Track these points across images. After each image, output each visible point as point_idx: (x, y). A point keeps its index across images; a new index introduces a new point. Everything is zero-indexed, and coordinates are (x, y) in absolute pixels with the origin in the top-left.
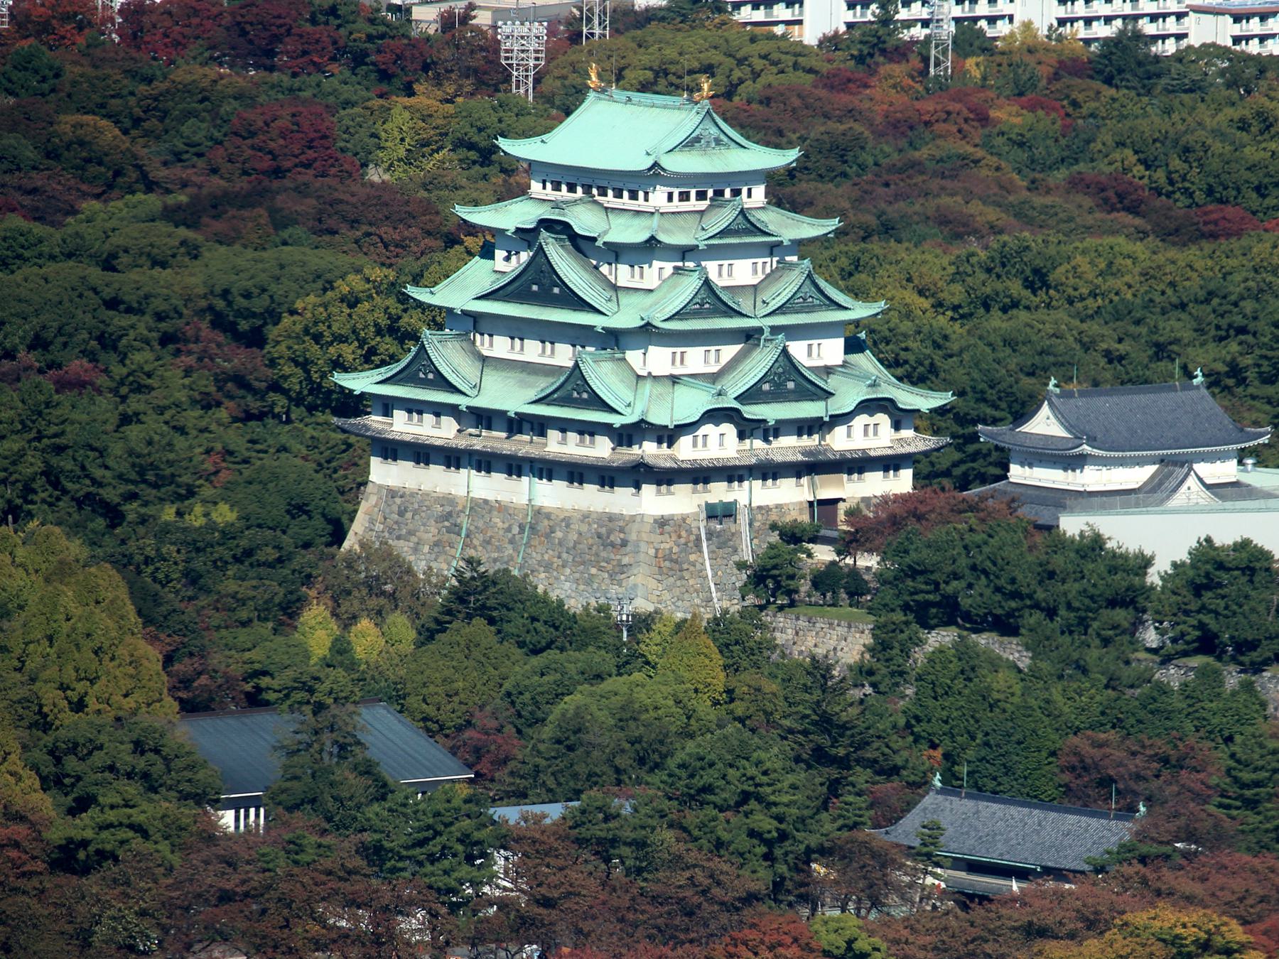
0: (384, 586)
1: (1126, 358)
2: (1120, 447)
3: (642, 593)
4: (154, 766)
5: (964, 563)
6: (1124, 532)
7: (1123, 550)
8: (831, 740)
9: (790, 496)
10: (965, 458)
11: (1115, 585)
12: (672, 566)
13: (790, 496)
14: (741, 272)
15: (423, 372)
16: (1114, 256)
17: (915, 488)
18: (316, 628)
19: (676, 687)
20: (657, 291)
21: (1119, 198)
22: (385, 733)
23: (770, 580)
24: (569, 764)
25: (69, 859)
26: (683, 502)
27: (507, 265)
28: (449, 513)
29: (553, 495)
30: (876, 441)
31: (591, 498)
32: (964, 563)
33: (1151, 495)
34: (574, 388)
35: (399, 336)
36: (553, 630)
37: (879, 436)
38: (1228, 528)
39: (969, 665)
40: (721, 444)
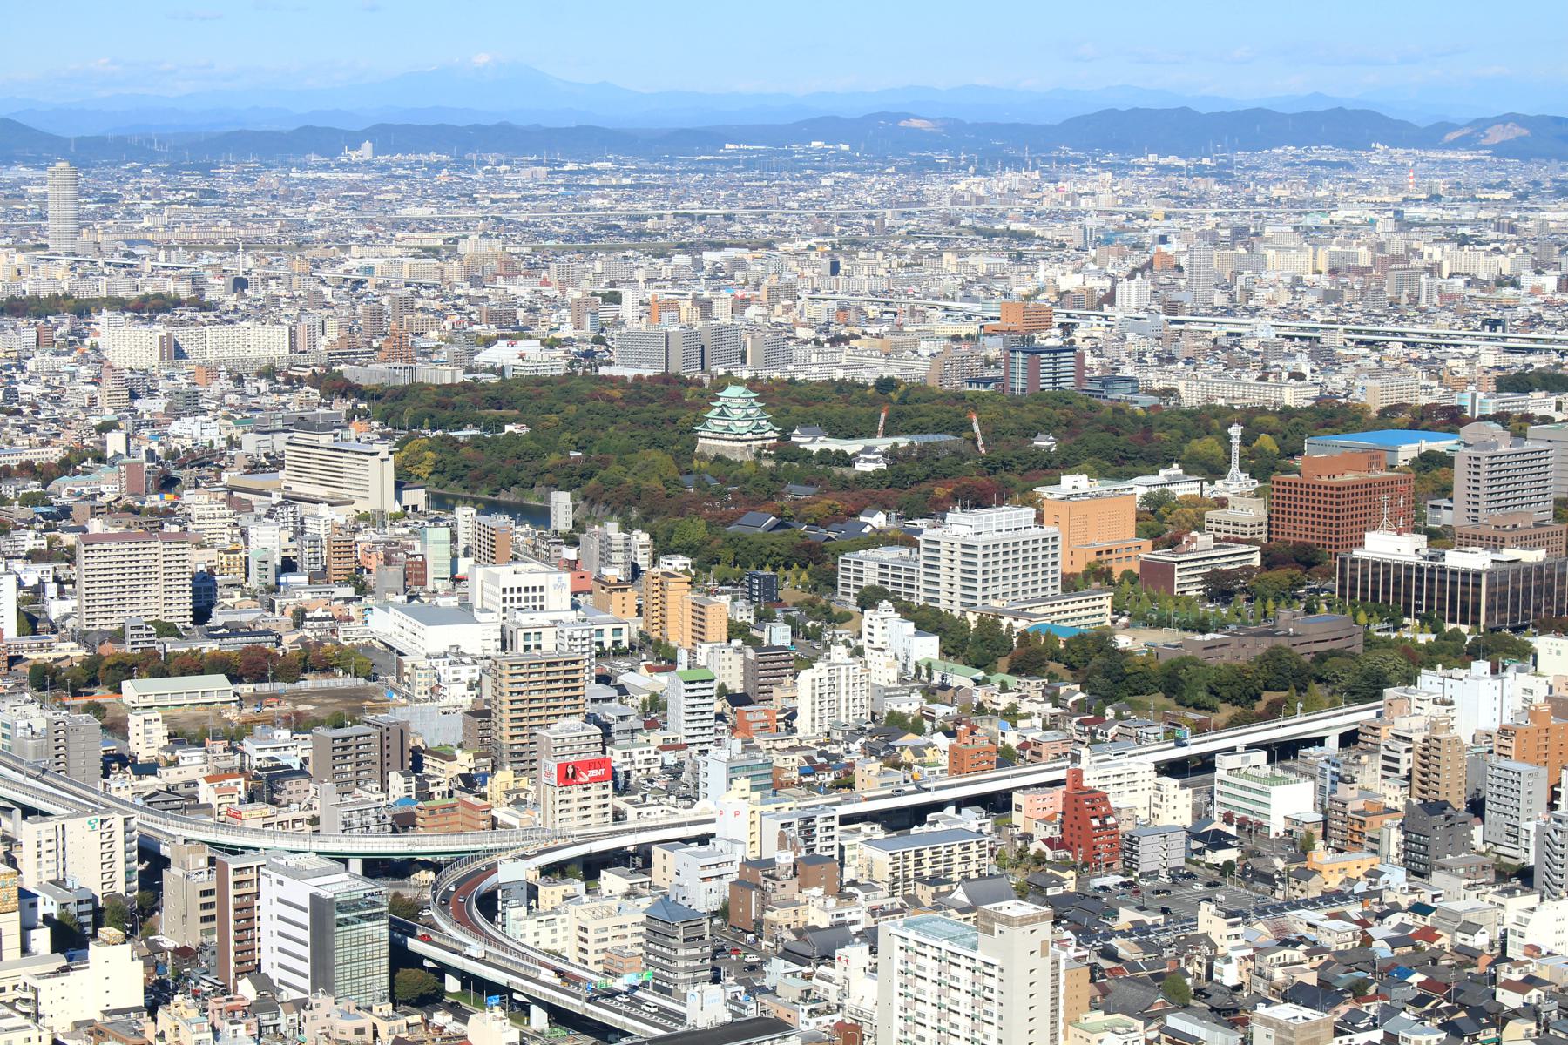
0: (703, 457)
1: (805, 423)
2: (806, 435)
3: (739, 458)
4: (677, 483)
5: (785, 451)
6: (809, 447)
7: (685, 904)
8: (774, 477)
9: (759, 443)
10: (784, 437)
11: (809, 455)
12: (743, 453)
13: (759, 443)
14: (751, 411)
15: (706, 427)
16: (797, 409)
17: (1419, 673)
18: (696, 463)
19: (746, 471)
20: (739, 414)
21: (795, 400)
22: (707, 477)
23: (758, 455)
24: (735, 482)
25: (668, 496)
26: (744, 444)
27: (718, 410)
28: (710, 447)
29: (725, 443)
30: (772, 434)
31: (731, 444)
32: (785, 451)
33: (812, 442)
34: (728, 428)
35: (702, 421)
36: (730, 463)
37: (771, 434)
38: (824, 446)
39: (791, 467)
40: (749, 436)
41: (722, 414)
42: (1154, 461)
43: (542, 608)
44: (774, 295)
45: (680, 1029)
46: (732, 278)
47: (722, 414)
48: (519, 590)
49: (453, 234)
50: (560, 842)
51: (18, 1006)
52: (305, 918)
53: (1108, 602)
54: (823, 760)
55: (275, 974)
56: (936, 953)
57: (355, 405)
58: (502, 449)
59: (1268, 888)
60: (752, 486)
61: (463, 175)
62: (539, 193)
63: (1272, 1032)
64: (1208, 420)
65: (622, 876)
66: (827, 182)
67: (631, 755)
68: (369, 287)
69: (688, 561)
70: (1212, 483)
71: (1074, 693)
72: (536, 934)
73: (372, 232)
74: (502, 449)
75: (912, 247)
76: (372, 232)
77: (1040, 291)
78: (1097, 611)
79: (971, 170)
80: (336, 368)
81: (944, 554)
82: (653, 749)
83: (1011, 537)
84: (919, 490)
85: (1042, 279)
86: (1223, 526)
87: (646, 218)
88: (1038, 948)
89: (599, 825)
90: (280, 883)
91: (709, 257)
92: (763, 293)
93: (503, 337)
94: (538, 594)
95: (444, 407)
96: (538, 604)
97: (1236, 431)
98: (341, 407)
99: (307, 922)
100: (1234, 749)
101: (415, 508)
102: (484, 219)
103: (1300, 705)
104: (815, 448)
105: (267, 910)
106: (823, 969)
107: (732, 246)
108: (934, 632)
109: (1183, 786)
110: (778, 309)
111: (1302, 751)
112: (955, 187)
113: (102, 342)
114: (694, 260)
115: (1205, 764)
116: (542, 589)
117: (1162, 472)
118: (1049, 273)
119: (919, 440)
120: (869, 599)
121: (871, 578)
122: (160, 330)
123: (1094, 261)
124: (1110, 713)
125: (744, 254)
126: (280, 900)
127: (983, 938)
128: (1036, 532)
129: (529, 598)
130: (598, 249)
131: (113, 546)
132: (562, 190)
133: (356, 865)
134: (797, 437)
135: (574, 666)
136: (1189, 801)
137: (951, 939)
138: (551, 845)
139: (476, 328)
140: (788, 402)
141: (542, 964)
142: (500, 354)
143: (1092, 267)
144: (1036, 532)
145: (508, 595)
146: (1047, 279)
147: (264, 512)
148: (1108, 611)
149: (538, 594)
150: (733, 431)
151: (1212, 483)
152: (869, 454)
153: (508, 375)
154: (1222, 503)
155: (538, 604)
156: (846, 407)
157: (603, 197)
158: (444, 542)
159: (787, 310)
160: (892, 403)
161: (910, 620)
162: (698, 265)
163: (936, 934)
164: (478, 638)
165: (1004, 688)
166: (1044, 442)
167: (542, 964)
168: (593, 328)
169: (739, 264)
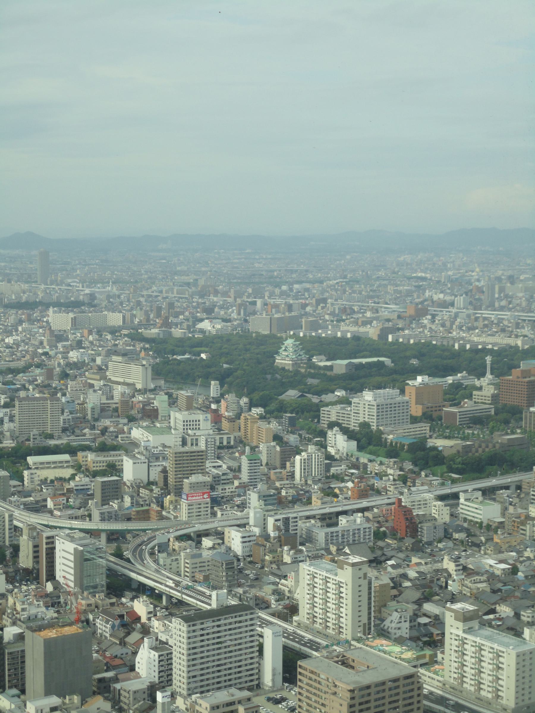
29: (286, 362)
35: (277, 353)
41: (285, 350)
42: (453, 371)
44: (318, 302)
45: (209, 607)
46: (304, 295)
47: (285, 350)
50: (187, 526)
52: (72, 558)
53: (428, 428)
54: (302, 492)
55: (62, 581)
56: (321, 577)
57: (144, 346)
58: (180, 366)
59: (477, 549)
60: (293, 379)
63: (453, 614)
64: (479, 353)
67: (225, 489)
70: (479, 379)
71: (408, 466)
72: (170, 565)
73: (165, 276)
74: (180, 366)
76: (165, 276)
80: (140, 331)
82: (234, 487)
83: (389, 401)
84: (356, 381)
86: (480, 397)
87: (273, 271)
88: (362, 576)
90: (63, 543)
91: (296, 286)
93: (207, 319)
94: (197, 423)
95: (179, 347)
97: (488, 359)
98: (139, 346)
99: (73, 559)
100: (467, 491)
103: (499, 472)
104: (322, 364)
105: (59, 554)
106: (283, 581)
108: (356, 440)
109: (446, 506)
110: (320, 308)
111: (498, 492)
113: (50, 320)
115: (455, 496)
116: (199, 421)
117: (459, 375)
118: (430, 294)
119: (375, 359)
120: (331, 425)
121: (333, 418)
122: (71, 315)
123: (449, 289)
125: (308, 286)
126: (63, 550)
127: (339, 571)
128: (400, 399)
129: (195, 425)
131: (42, 402)
132: (243, 260)
133: (104, 536)
134: (314, 360)
135: (201, 454)
136: (448, 512)
137: (327, 571)
138: (183, 527)
139: (198, 314)
141: (168, 577)
142: (206, 325)
143: (448, 291)
145: (185, 423)
147: (98, 388)
148: (428, 432)
149: (197, 423)
150: (286, 358)
151: (479, 379)
153: (207, 334)
154: (480, 389)
156: (334, 348)
157: (259, 263)
158: (165, 401)
162: (291, 290)
163: (321, 569)
164: (172, 440)
165: (381, 463)
167: (168, 577)
168: (245, 314)
169: (307, 290)
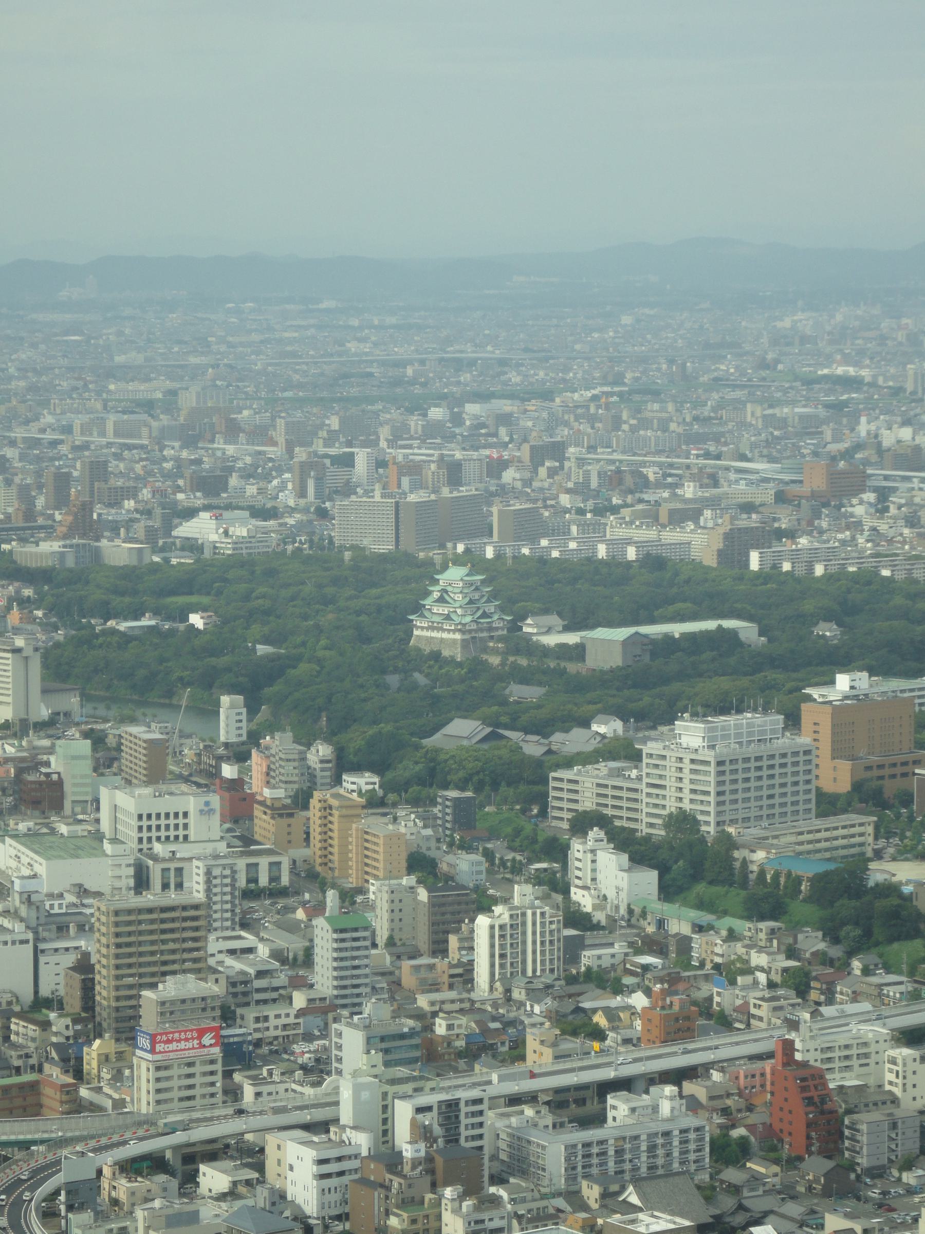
29: (445, 635)
35: (418, 609)
41: (441, 600)
43: (186, 837)
44: (539, 455)
46: (495, 435)
47: (441, 600)
48: (167, 815)
49: (176, 385)
51: (368, 990)
57: (18, 592)
60: (469, 685)
61: (199, 315)
62: (286, 335)
65: (224, 1172)
66: (626, 320)
67: (266, 1018)
68: (64, 449)
69: (376, 779)
71: (813, 942)
75: (715, 396)
77: (858, 447)
78: (857, 840)
79: (800, 303)
81: (671, 773)
82: (293, 1012)
83: (752, 750)
84: (652, 691)
85: (863, 434)
89: (204, 1108)
91: (472, 409)
92: (525, 453)
93: (206, 508)
94: (181, 821)
96: (181, 833)
101: (67, 714)
102: (215, 366)
104: (551, 640)
107: (503, 396)
108: (653, 867)
110: (542, 472)
112: (779, 324)
114: (453, 414)
116: (185, 815)
118: (873, 427)
120: (582, 824)
124: (856, 965)
125: (506, 406)
128: (785, 742)
129: (173, 827)
130: (300, 386)
132: (313, 331)
134: (529, 627)
140: (521, 587)
142: (203, 528)
144: (785, 742)
145: (145, 823)
146: (868, 433)
149: (181, 821)
152: (608, 643)
153: (207, 554)
155: (181, 833)
156: (587, 592)
159: (552, 473)
160: (657, 585)
161: (625, 852)
162: (457, 419)
166: (828, 631)
169: (505, 419)
